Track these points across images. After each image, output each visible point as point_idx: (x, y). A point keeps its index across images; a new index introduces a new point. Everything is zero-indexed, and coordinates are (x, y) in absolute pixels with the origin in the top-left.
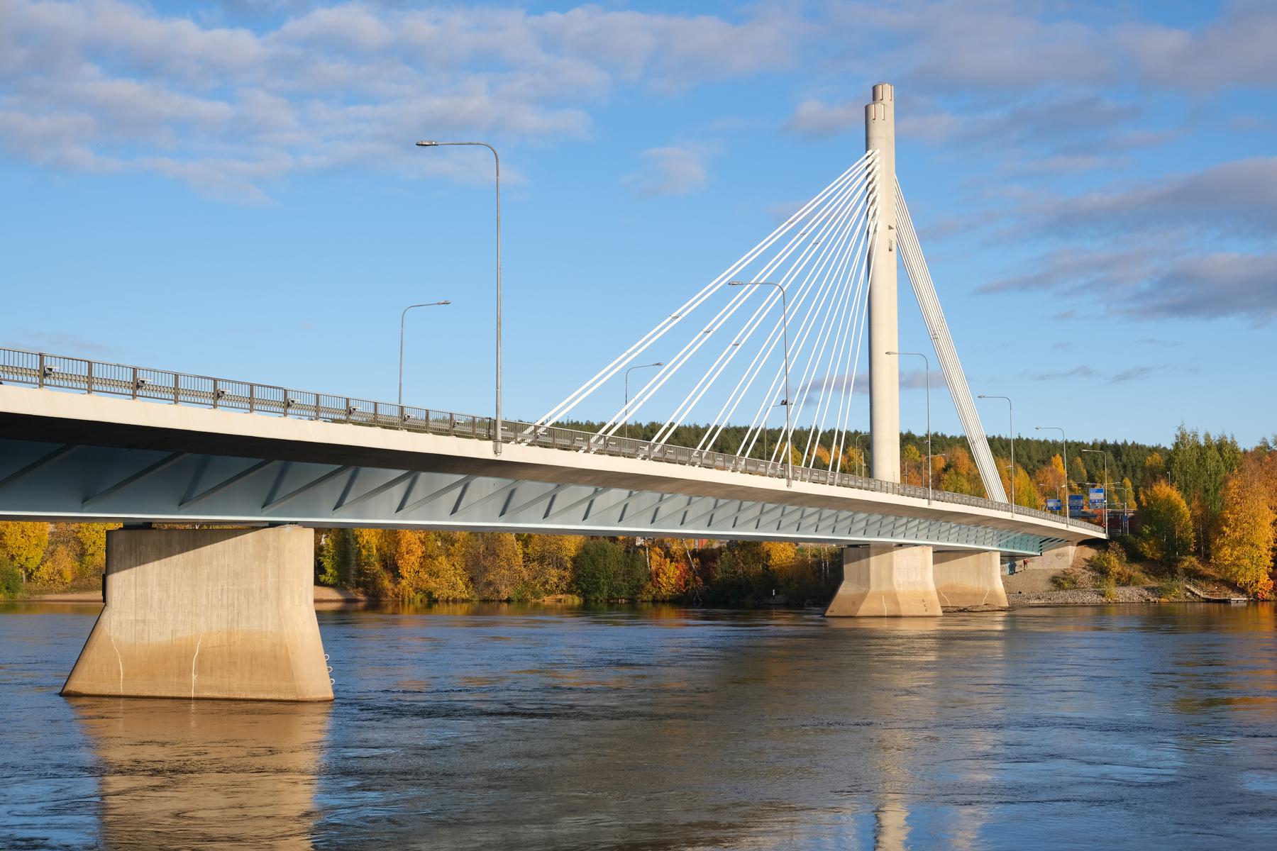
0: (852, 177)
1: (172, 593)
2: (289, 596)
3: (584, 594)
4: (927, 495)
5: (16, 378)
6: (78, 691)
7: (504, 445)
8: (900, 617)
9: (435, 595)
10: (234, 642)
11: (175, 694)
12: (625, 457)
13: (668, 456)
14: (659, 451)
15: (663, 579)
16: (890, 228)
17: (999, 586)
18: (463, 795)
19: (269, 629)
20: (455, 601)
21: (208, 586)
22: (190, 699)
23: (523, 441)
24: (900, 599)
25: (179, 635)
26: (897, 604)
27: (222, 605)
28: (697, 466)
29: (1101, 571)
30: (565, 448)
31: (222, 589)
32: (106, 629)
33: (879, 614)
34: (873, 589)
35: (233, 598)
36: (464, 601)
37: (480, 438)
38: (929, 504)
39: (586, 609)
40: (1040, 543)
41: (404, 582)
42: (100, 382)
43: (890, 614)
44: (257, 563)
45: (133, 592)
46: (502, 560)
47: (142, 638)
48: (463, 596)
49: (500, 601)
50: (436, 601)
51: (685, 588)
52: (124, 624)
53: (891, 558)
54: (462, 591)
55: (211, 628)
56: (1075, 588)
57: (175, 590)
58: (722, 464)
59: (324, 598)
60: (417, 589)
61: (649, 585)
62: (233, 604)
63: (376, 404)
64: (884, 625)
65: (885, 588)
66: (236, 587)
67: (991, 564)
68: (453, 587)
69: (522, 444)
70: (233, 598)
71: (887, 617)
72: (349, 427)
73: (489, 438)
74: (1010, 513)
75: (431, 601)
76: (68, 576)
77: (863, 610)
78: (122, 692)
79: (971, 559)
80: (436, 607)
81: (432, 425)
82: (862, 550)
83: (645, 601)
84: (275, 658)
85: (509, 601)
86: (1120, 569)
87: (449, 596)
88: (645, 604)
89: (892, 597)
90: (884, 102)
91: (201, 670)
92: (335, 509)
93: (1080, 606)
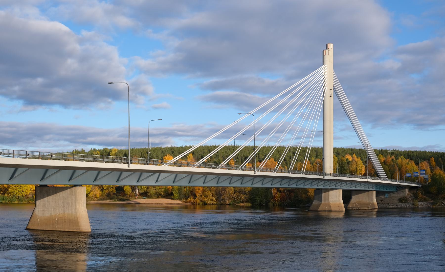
1: (50, 203)
2: (78, 205)
3: (252, 202)
4: (254, 169)
5: (9, 156)
6: (29, 228)
7: (131, 164)
8: (331, 211)
9: (206, 202)
10: (65, 216)
11: (52, 230)
12: (148, 165)
13: (212, 167)
14: (262, 169)
17: (375, 201)
18: (385, 235)
19: (73, 213)
20: (212, 204)
21: (59, 202)
22: (55, 231)
23: (219, 168)
24: (331, 205)
25: (52, 214)
26: (330, 207)
27: (62, 207)
28: (273, 172)
30: (209, 168)
31: (62, 203)
32: (35, 212)
33: (324, 210)
34: (323, 202)
35: (65, 205)
36: (215, 204)
37: (124, 163)
38: (324, 177)
39: (253, 208)
40: (397, 188)
42: (18, 155)
43: (328, 210)
44: (70, 196)
45: (41, 203)
47: (44, 215)
48: (215, 203)
49: (226, 204)
50: (207, 204)
52: (39, 211)
53: (372, 193)
54: (214, 201)
55: (60, 213)
56: (406, 202)
57: (51, 203)
58: (320, 174)
59: (173, 203)
60: (201, 201)
61: (272, 200)
62: (65, 207)
63: (13, 151)
64: (326, 214)
65: (326, 202)
66: (65, 202)
67: (372, 195)
68: (212, 200)
69: (219, 169)
70: (65, 205)
71: (328, 211)
72: (267, 173)
73: (253, 171)
75: (205, 204)
76: (98, 195)
77: (320, 209)
78: (39, 229)
79: (366, 193)
80: (206, 206)
81: (41, 156)
82: (327, 190)
83: (271, 205)
84: (75, 220)
85: (229, 204)
86: (422, 196)
87: (210, 203)
88: (271, 206)
89: (329, 205)
91: (57, 224)
92: (69, 181)
93: (403, 208)
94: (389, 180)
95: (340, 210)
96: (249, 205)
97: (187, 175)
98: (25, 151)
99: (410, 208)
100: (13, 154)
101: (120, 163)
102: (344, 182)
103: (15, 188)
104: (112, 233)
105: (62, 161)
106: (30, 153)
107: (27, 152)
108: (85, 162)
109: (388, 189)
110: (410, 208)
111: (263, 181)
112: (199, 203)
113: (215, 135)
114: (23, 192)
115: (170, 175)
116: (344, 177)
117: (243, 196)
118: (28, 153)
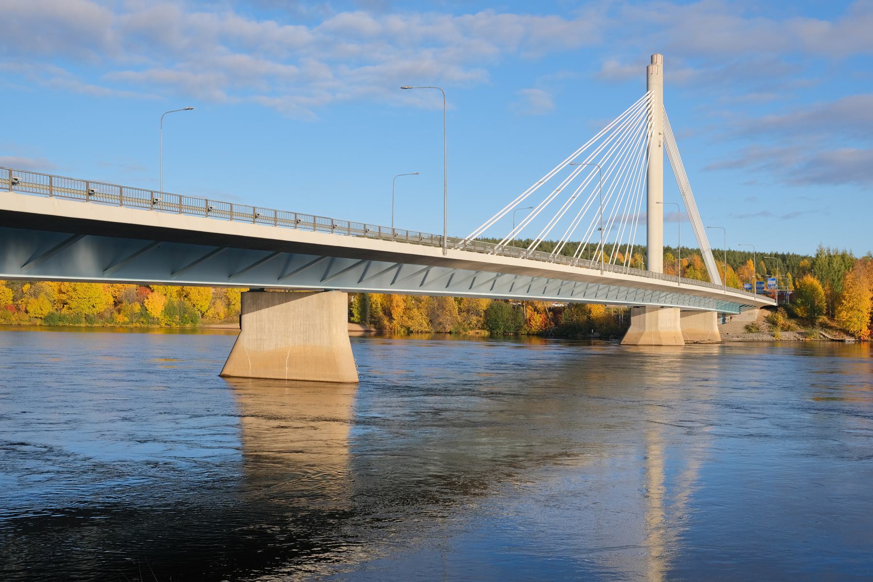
0: (638, 106)
13: (536, 257)
15: (533, 323)
16: (660, 134)
17: (716, 330)
20: (422, 332)
23: (458, 248)
24: (662, 336)
26: (660, 338)
28: (489, 254)
29: (773, 323)
34: (647, 330)
37: (435, 246)
41: (395, 322)
46: (447, 311)
49: (446, 333)
50: (412, 332)
51: (545, 328)
54: (425, 327)
55: (295, 344)
61: (525, 326)
68: (421, 325)
69: (458, 250)
71: (655, 345)
74: (723, 291)
75: (409, 332)
76: (222, 315)
79: (701, 315)
81: (409, 239)
82: (641, 309)
83: (523, 334)
85: (450, 333)
88: (523, 336)
90: (658, 64)
94: (631, 271)
95: (677, 344)
96: (486, 333)
97: (426, 272)
98: (228, 204)
99: (767, 342)
100: (349, 229)
101: (429, 246)
102: (352, 261)
103: (80, 300)
104: (434, 375)
105: (474, 253)
106: (215, 205)
107: (10, 171)
108: (561, 265)
109: (681, 303)
110: (767, 342)
111: (495, 280)
112: (399, 329)
113: (603, 133)
114: (94, 307)
115: (595, 285)
116: (561, 265)
117: (474, 319)
118: (90, 187)
